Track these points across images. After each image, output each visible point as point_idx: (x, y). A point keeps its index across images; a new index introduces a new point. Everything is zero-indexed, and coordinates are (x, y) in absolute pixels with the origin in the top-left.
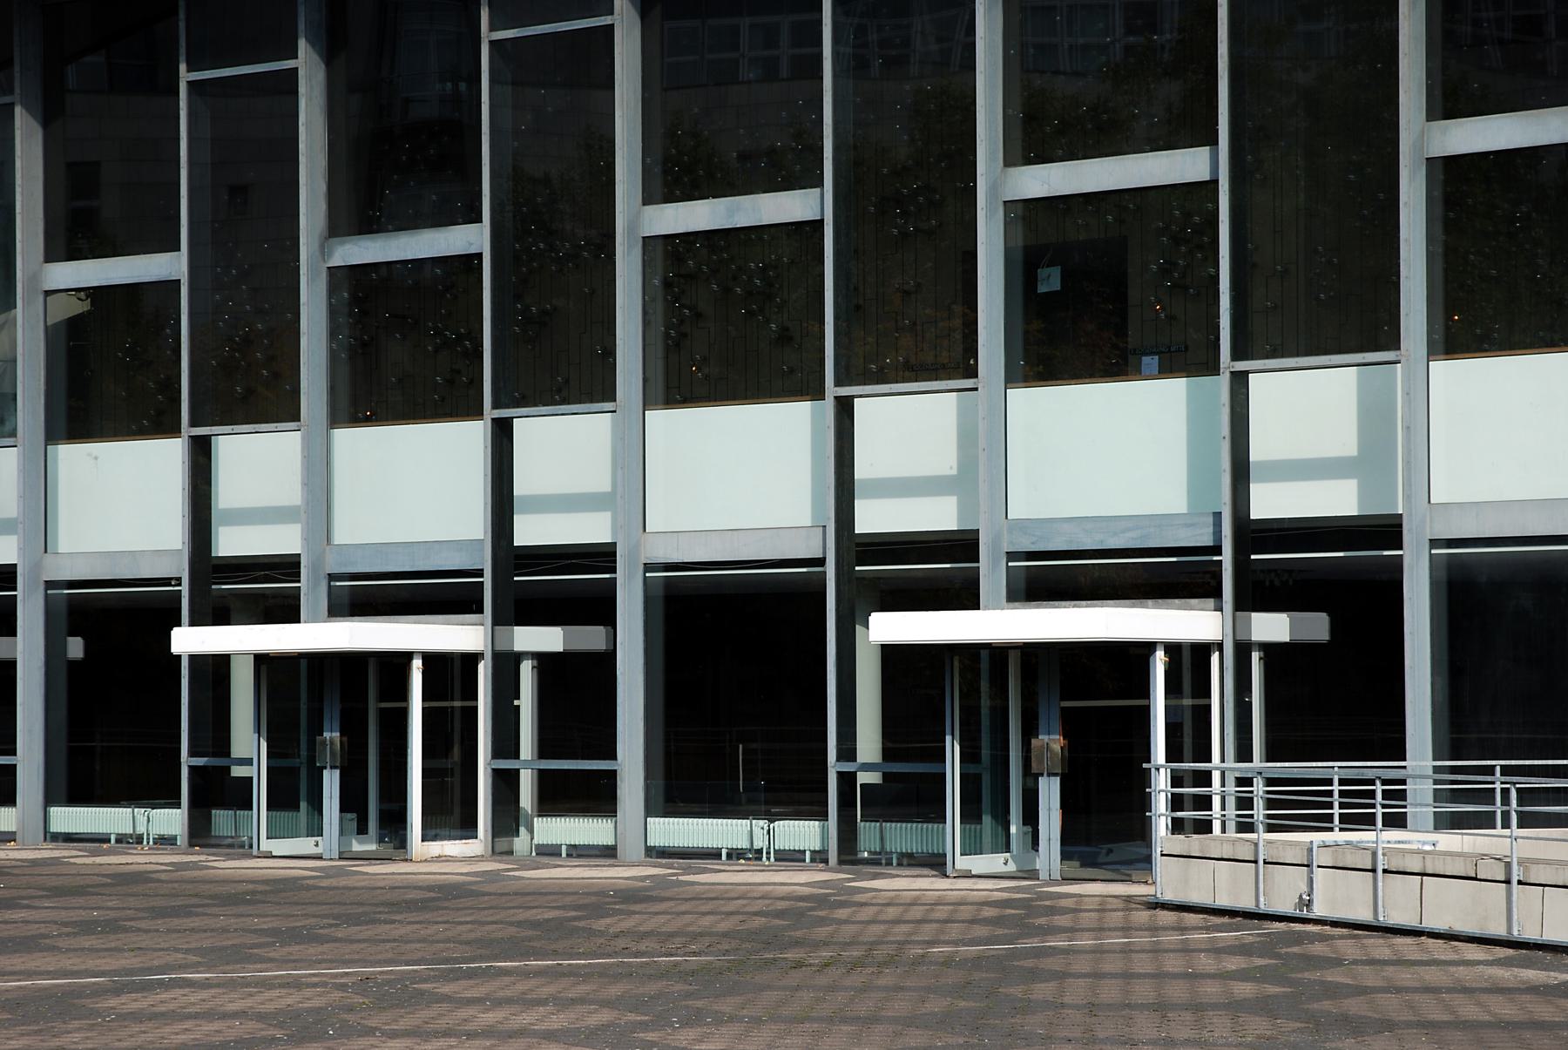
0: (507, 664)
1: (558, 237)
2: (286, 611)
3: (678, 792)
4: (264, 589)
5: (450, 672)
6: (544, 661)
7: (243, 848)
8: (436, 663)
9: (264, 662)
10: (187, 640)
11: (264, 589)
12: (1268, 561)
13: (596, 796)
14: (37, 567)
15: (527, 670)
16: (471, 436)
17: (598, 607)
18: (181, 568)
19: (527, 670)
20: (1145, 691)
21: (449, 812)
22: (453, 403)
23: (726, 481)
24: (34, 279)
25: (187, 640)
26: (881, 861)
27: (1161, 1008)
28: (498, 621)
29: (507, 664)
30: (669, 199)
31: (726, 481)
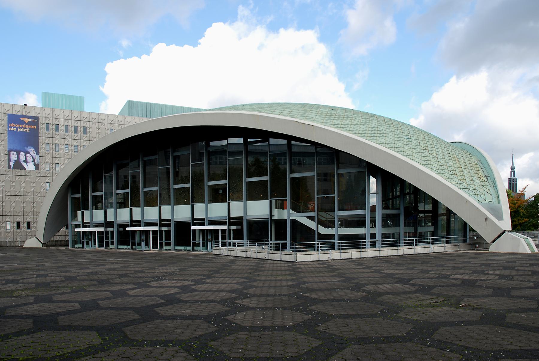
0: (161, 232)
1: (135, 191)
2: (203, 224)
3: (177, 244)
4: (201, 222)
5: (154, 232)
6: (165, 231)
7: (135, 249)
8: (153, 231)
9: (200, 230)
10: (193, 228)
11: (201, 222)
12: (232, 221)
13: (168, 244)
14: (173, 220)
15: (109, 233)
16: (189, 206)
17: (169, 225)
18: (81, 223)
19: (109, 233)
20: (219, 234)
21: (155, 246)
22: (223, 201)
23: (182, 213)
24: (115, 192)
25: (193, 228)
26: (196, 251)
27: (308, 272)
28: (229, 225)
29: (230, 230)
30: (211, 181)
31: (182, 213)
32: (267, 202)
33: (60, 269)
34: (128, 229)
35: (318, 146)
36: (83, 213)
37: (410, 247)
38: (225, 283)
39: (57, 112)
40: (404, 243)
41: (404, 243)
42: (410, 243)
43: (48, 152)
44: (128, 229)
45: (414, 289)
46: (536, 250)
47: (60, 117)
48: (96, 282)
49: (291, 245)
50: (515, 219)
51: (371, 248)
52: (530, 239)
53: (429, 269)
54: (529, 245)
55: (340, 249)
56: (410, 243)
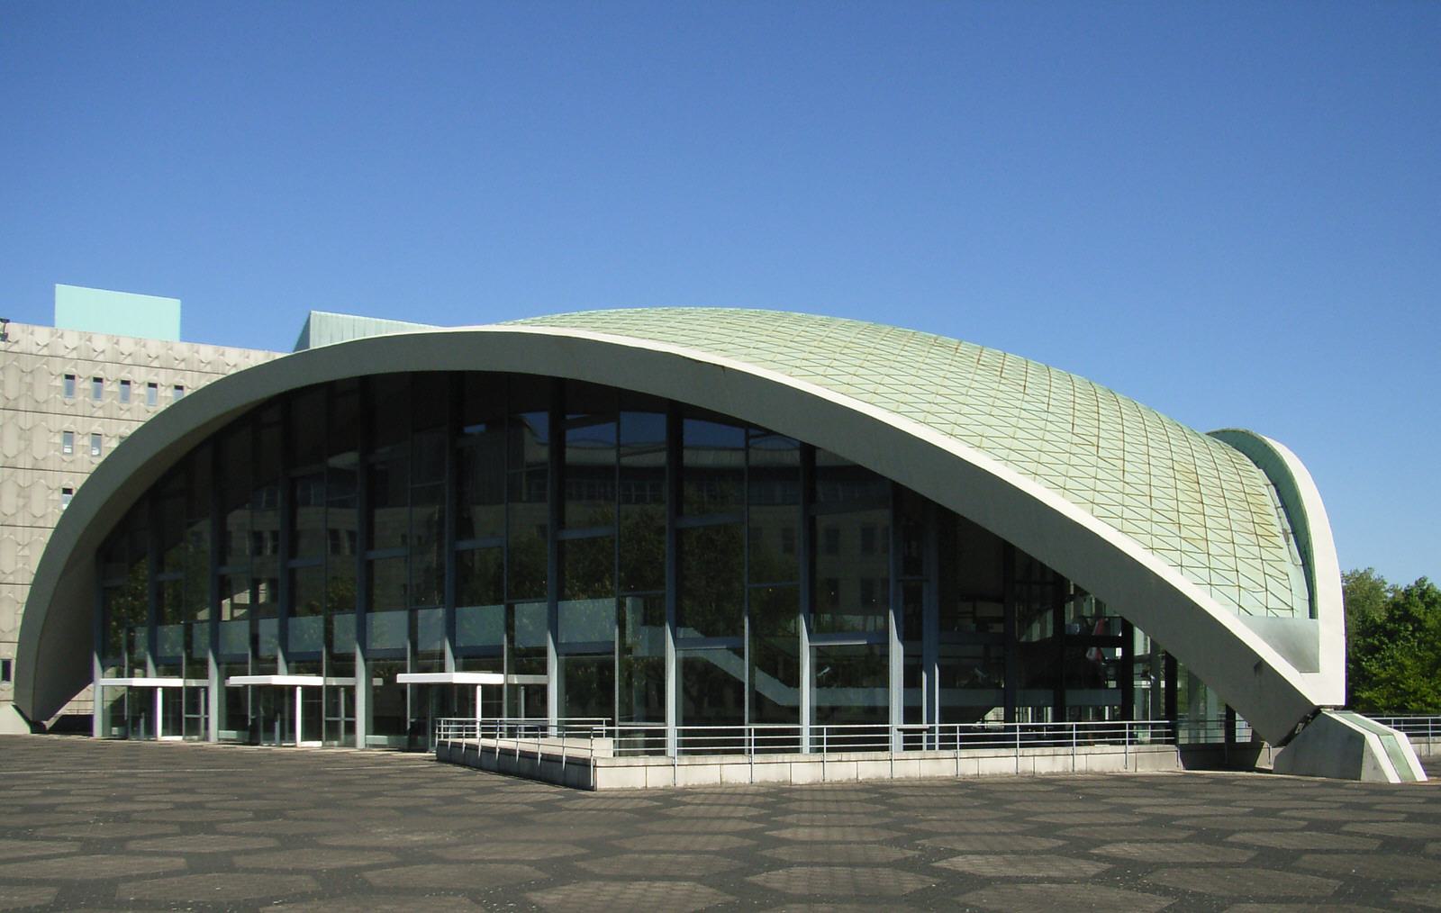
32: (609, 604)
33: (170, 785)
34: (402, 678)
35: (752, 432)
36: (1146, 651)
37: (1003, 752)
38: (697, 834)
39: (100, 343)
40: (757, 742)
41: (742, 742)
42: (1004, 738)
43: (70, 458)
44: (402, 678)
45: (1245, 859)
46: (1420, 776)
47: (109, 356)
48: (176, 829)
49: (812, 731)
50: (1373, 667)
51: (906, 748)
52: (1401, 737)
53: (1275, 805)
54: (1394, 755)
55: (820, 750)
56: (1004, 738)
